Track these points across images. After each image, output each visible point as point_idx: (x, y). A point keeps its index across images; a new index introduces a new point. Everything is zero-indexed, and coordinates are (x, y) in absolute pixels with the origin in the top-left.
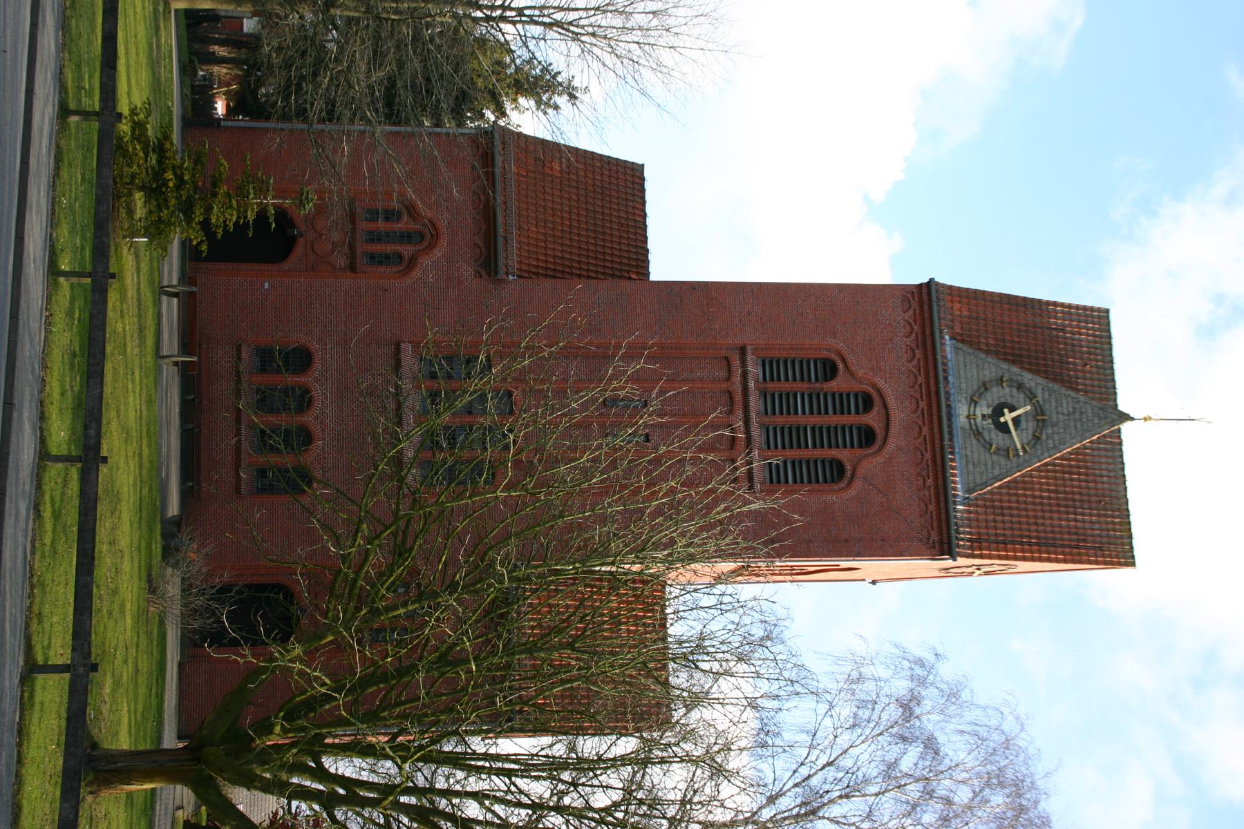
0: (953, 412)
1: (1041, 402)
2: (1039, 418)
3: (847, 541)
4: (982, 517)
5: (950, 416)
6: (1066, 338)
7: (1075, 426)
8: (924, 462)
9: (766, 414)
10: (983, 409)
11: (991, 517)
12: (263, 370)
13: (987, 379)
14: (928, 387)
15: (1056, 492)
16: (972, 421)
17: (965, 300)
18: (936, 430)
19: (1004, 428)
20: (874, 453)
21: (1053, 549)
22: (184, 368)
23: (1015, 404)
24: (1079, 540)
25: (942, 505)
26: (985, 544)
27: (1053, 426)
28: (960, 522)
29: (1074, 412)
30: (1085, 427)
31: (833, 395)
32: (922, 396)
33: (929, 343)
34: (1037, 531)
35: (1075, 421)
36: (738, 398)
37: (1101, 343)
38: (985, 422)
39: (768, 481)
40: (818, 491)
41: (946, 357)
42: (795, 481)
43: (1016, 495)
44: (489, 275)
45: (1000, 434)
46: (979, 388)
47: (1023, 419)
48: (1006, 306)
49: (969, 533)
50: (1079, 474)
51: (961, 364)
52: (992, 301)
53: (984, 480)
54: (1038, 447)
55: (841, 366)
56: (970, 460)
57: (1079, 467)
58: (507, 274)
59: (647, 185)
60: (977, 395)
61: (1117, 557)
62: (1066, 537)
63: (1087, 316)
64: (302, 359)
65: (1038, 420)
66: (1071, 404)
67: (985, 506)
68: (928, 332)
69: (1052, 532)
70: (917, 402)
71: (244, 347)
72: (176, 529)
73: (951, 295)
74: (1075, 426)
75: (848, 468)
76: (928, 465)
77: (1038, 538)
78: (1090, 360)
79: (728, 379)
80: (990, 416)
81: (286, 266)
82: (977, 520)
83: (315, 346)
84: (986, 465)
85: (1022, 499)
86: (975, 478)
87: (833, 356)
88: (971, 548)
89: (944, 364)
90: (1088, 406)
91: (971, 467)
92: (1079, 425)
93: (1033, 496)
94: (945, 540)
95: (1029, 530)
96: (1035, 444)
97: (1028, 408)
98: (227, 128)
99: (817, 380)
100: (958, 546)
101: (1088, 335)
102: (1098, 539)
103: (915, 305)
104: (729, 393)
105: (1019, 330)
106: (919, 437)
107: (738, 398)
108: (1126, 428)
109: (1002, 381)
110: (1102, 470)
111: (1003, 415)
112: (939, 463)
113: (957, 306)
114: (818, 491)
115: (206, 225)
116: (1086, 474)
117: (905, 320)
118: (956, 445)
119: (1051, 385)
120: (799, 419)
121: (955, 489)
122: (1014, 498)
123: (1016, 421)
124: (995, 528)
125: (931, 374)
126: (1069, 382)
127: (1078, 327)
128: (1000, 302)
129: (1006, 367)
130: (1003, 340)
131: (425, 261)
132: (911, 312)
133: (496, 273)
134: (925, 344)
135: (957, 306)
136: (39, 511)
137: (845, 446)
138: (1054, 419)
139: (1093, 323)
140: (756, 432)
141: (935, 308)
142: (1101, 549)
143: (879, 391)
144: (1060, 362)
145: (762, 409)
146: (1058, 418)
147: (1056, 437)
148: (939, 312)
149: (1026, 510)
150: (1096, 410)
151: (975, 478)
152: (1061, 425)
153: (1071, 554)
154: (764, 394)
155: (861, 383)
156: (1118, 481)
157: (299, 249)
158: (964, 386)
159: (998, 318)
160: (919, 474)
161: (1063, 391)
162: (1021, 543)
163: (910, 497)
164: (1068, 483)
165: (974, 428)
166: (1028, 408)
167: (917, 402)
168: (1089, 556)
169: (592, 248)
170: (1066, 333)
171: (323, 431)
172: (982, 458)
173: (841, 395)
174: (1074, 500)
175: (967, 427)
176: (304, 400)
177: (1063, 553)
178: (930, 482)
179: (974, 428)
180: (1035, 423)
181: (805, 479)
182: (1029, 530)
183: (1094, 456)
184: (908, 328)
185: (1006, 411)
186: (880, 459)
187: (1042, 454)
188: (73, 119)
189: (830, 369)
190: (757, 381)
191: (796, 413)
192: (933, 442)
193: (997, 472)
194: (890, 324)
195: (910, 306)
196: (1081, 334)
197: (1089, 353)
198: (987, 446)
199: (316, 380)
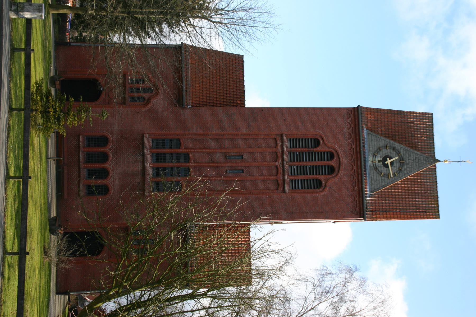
0: (366, 159)
1: (402, 155)
2: (401, 162)
3: (322, 212)
4: (377, 202)
5: (365, 161)
6: (414, 126)
7: (416, 165)
8: (354, 180)
9: (291, 161)
10: (379, 158)
11: (380, 202)
12: (89, 145)
13: (381, 146)
14: (356, 150)
15: (408, 190)
16: (374, 163)
17: (373, 113)
18: (359, 167)
19: (387, 166)
20: (334, 177)
21: (405, 213)
22: (57, 163)
23: (391, 156)
24: (416, 209)
25: (361, 198)
26: (378, 213)
27: (407, 165)
28: (368, 204)
29: (416, 159)
30: (420, 165)
31: (318, 153)
32: (354, 153)
33: (357, 132)
34: (399, 206)
35: (416, 163)
36: (280, 155)
37: (429, 127)
38: (379, 164)
39: (291, 188)
40: (311, 192)
41: (364, 137)
42: (302, 188)
43: (391, 192)
44: (180, 106)
45: (385, 168)
46: (377, 150)
47: (395, 162)
48: (390, 115)
49: (372, 209)
50: (418, 182)
51: (370, 140)
52: (384, 113)
53: (378, 187)
54: (401, 173)
55: (321, 141)
56: (373, 179)
57: (418, 179)
58: (187, 105)
59: (245, 64)
60: (376, 152)
61: (432, 215)
62: (411, 208)
63: (423, 117)
64: (104, 141)
65: (401, 163)
66: (414, 156)
67: (378, 197)
68: (357, 127)
69: (406, 206)
70: (352, 156)
71: (81, 137)
72: (54, 222)
73: (367, 111)
74: (416, 165)
75: (324, 183)
76: (355, 181)
77: (400, 209)
78: (424, 135)
79: (276, 147)
80: (381, 161)
81: (98, 103)
82: (375, 203)
83: (109, 136)
84: (379, 181)
85: (393, 193)
86: (374, 186)
87: (318, 137)
88: (372, 215)
89: (363, 140)
90: (421, 156)
91: (373, 182)
92: (417, 165)
93: (398, 192)
94: (362, 212)
95: (396, 206)
96: (399, 172)
97: (397, 158)
98: (73, 46)
99: (312, 147)
100: (367, 214)
101: (424, 124)
102: (424, 208)
103: (352, 116)
104: (276, 152)
105: (395, 124)
106: (352, 170)
107: (280, 155)
108: (438, 164)
109: (387, 147)
110: (427, 180)
111: (387, 160)
112: (360, 180)
113: (369, 116)
114: (311, 192)
115: (66, 126)
116: (421, 182)
117: (348, 123)
118: (367, 173)
119: (406, 148)
120: (304, 163)
121: (366, 188)
122: (390, 193)
123: (392, 163)
124: (382, 206)
125: (358, 145)
126: (415, 147)
127: (420, 121)
128: (387, 113)
129: (388, 141)
130: (388, 129)
131: (154, 100)
132: (350, 119)
133: (183, 105)
134: (355, 132)
135: (369, 116)
136: (3, 275)
137: (322, 174)
138: (408, 162)
139: (426, 119)
140: (287, 169)
141: (360, 117)
142: (425, 212)
143: (336, 151)
144: (411, 136)
145: (289, 159)
146: (409, 162)
147: (408, 169)
148: (362, 119)
149: (395, 198)
150: (425, 158)
151: (374, 186)
152: (410, 164)
153: (413, 215)
154: (290, 153)
155: (329, 148)
156: (434, 184)
157: (103, 96)
158: (371, 149)
159: (386, 120)
160: (352, 185)
161: (411, 150)
162: (393, 211)
163: (348, 194)
164: (413, 186)
165: (375, 166)
166: (397, 158)
167: (352, 156)
168: (421, 215)
169: (222, 97)
170: (414, 124)
171: (113, 170)
172: (378, 178)
173: (321, 153)
174: (415, 193)
175: (372, 166)
176: (105, 157)
177: (410, 215)
178: (356, 188)
179: (375, 166)
180: (400, 164)
181: (306, 188)
182: (396, 206)
183: (424, 174)
184: (349, 125)
185: (388, 159)
186: (336, 179)
187: (402, 176)
188: (15, 112)
189: (317, 143)
190: (287, 148)
191: (303, 161)
192: (358, 172)
193: (383, 184)
194: (342, 124)
195: (350, 116)
196: (420, 124)
197: (424, 132)
198: (380, 173)
199: (110, 149)
